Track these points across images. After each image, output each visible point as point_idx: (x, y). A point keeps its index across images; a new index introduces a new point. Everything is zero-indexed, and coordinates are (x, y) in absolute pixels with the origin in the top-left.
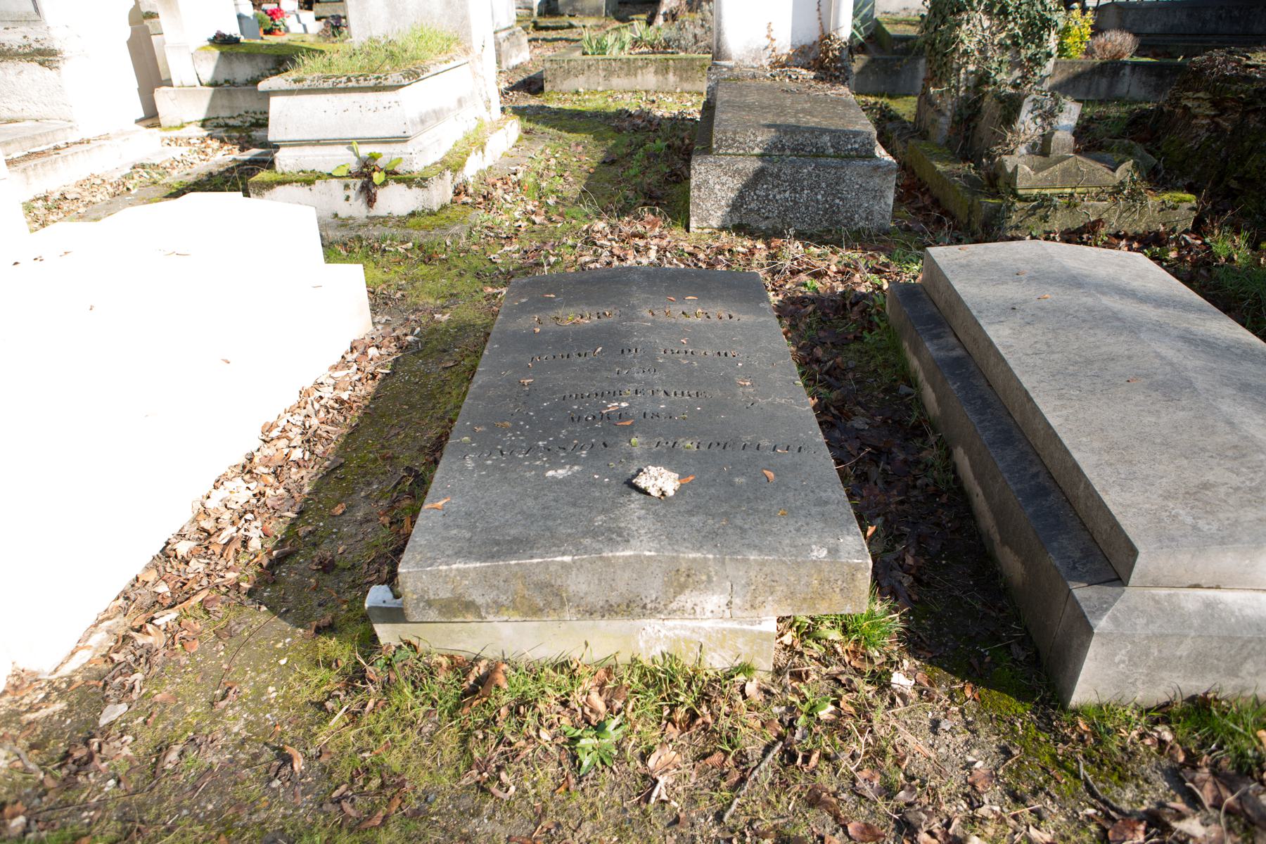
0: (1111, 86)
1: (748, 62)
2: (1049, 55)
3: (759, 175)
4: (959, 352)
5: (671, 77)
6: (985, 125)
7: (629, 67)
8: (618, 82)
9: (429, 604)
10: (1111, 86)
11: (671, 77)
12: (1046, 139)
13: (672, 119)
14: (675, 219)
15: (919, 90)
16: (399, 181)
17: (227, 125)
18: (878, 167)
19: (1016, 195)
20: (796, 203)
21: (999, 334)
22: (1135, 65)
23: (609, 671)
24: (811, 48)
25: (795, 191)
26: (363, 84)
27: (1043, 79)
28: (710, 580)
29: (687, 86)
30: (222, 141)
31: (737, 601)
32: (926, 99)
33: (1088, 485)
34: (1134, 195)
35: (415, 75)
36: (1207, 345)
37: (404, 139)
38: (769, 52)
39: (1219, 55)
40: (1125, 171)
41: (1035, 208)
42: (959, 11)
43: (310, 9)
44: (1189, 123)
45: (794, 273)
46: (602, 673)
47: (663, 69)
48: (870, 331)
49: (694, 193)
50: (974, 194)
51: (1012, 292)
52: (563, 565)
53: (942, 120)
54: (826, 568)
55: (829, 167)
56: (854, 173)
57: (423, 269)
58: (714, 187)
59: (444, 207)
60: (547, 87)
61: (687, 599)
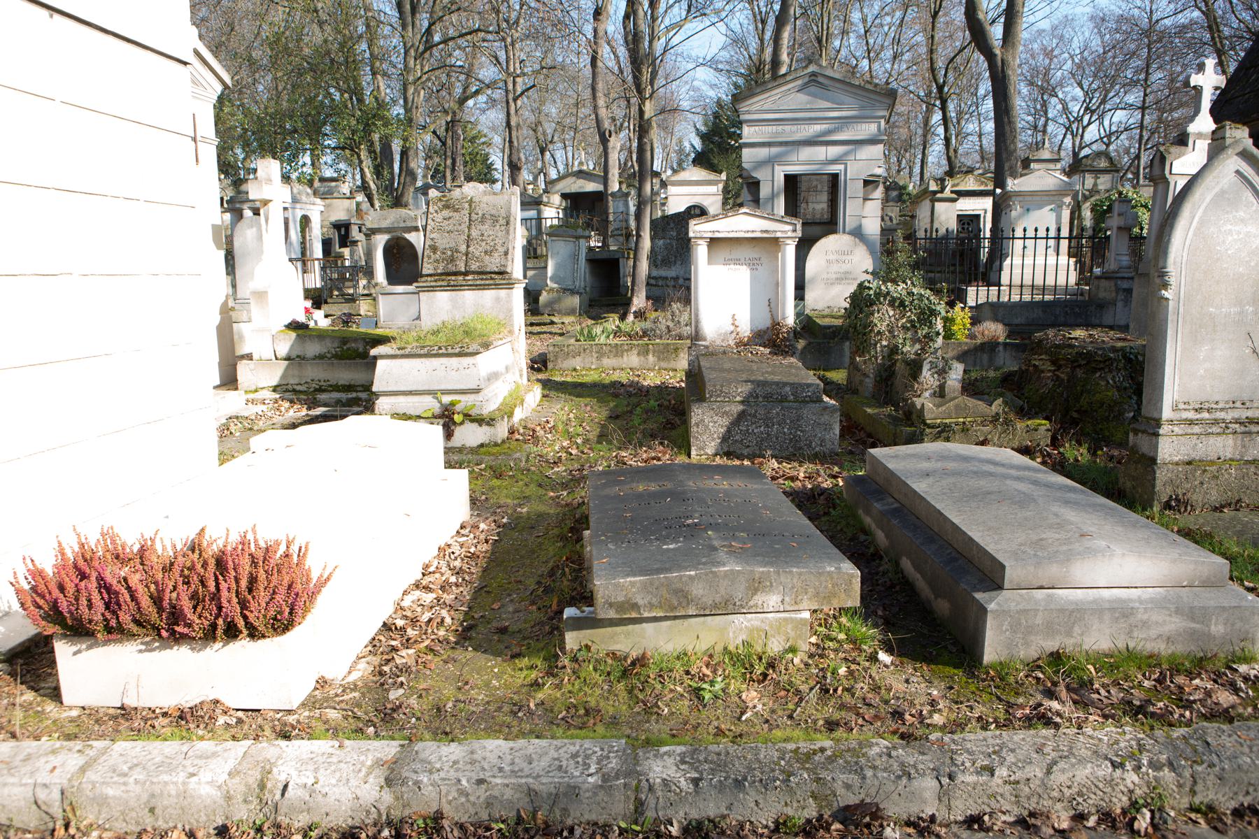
0: (991, 360)
1: (718, 342)
2: (938, 334)
3: (742, 415)
4: (896, 505)
5: (651, 358)
6: (899, 381)
7: (618, 351)
8: (607, 362)
9: (611, 605)
10: (991, 360)
11: (651, 358)
12: (942, 387)
13: (657, 387)
14: (680, 448)
15: (847, 360)
16: (473, 421)
17: (294, 390)
18: (826, 408)
19: (925, 424)
20: (769, 435)
21: (920, 486)
22: (1005, 344)
23: (711, 656)
24: (765, 332)
25: (767, 426)
26: (450, 351)
27: (936, 350)
28: (771, 585)
29: (664, 365)
30: (292, 401)
31: (787, 599)
32: (854, 367)
33: (978, 545)
34: (1007, 422)
35: (486, 346)
36: (1048, 486)
37: (477, 391)
38: (734, 335)
39: (1051, 333)
40: (997, 406)
41: (940, 433)
42: (871, 305)
43: (319, 308)
44: (1039, 377)
45: (773, 478)
46: (706, 658)
47: (644, 352)
48: (834, 508)
49: (694, 429)
50: (896, 426)
51: (925, 465)
52: (690, 577)
53: (867, 380)
54: (835, 576)
55: (791, 408)
56: (808, 412)
57: (496, 482)
58: (708, 428)
59: (503, 442)
60: (550, 365)
61: (759, 599)
